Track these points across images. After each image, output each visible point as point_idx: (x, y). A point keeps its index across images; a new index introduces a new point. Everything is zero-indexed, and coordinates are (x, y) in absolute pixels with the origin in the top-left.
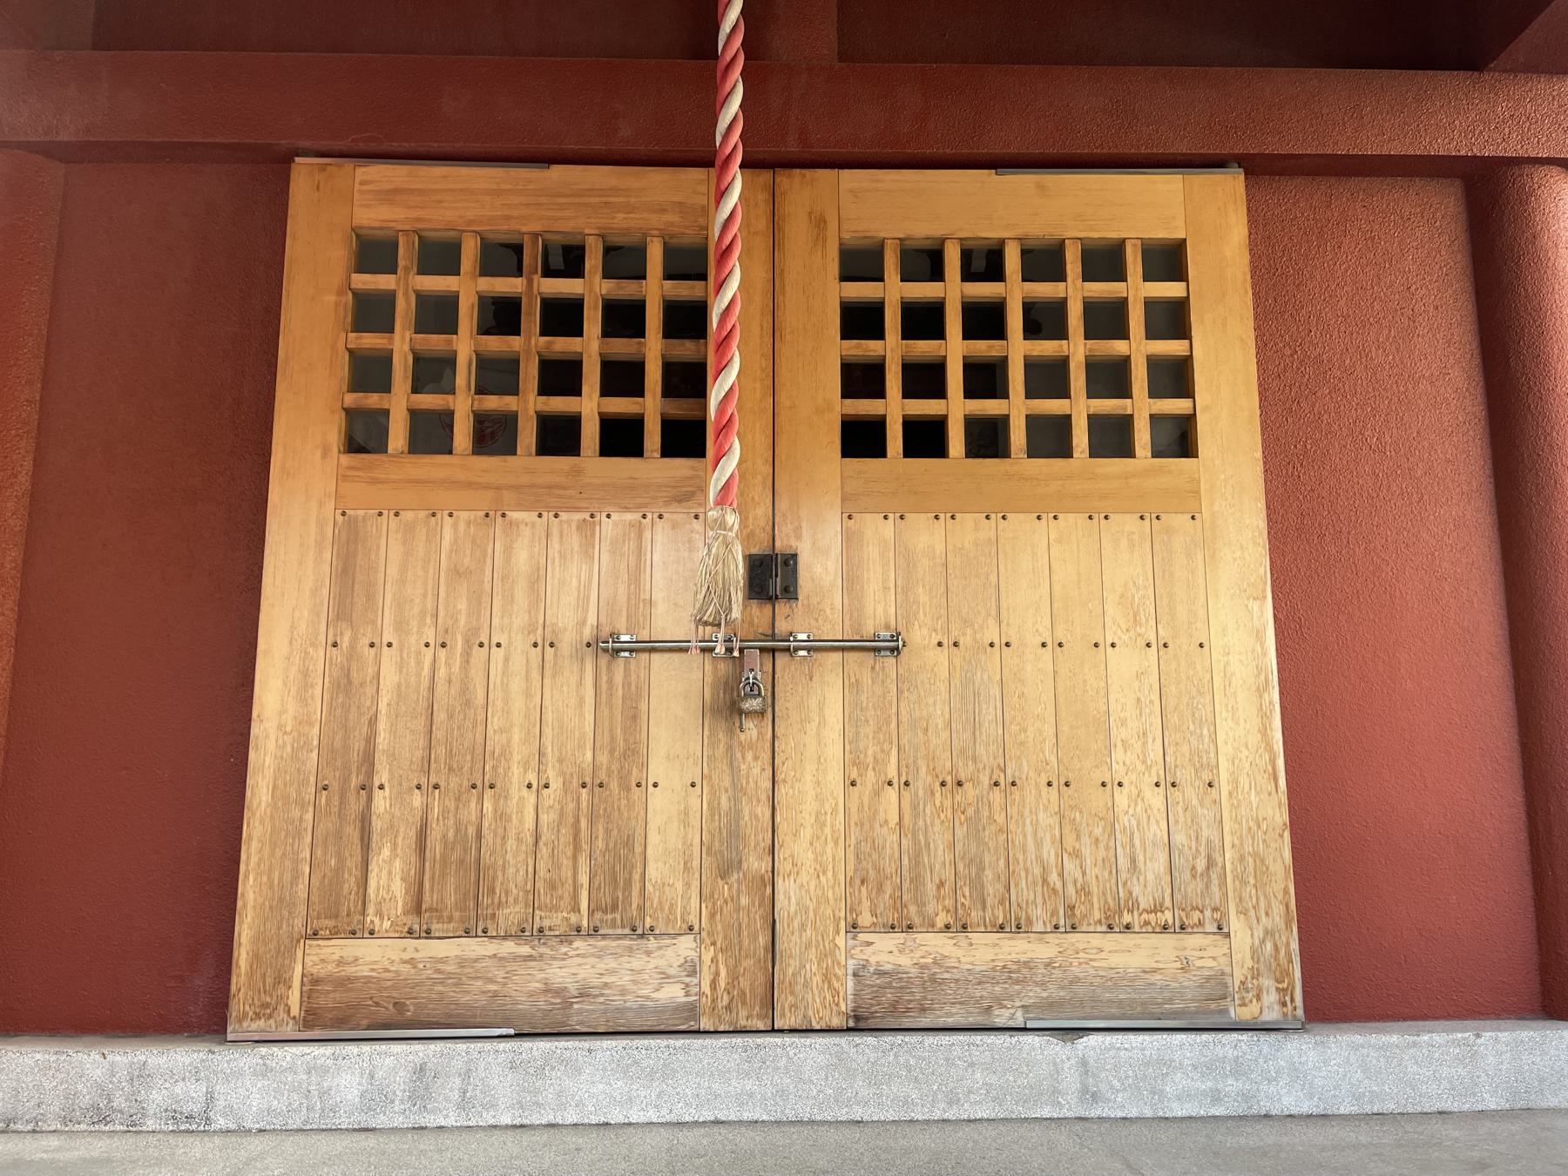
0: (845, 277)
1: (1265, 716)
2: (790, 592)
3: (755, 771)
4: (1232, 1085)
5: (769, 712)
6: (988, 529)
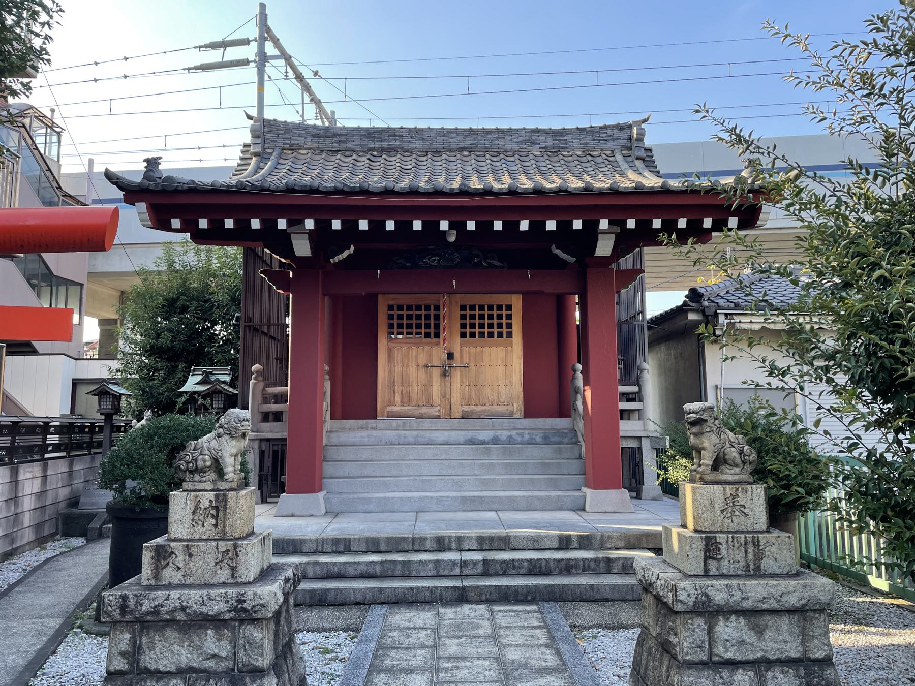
2: (453, 358)
3: (448, 384)
5: (450, 375)
6: (482, 349)
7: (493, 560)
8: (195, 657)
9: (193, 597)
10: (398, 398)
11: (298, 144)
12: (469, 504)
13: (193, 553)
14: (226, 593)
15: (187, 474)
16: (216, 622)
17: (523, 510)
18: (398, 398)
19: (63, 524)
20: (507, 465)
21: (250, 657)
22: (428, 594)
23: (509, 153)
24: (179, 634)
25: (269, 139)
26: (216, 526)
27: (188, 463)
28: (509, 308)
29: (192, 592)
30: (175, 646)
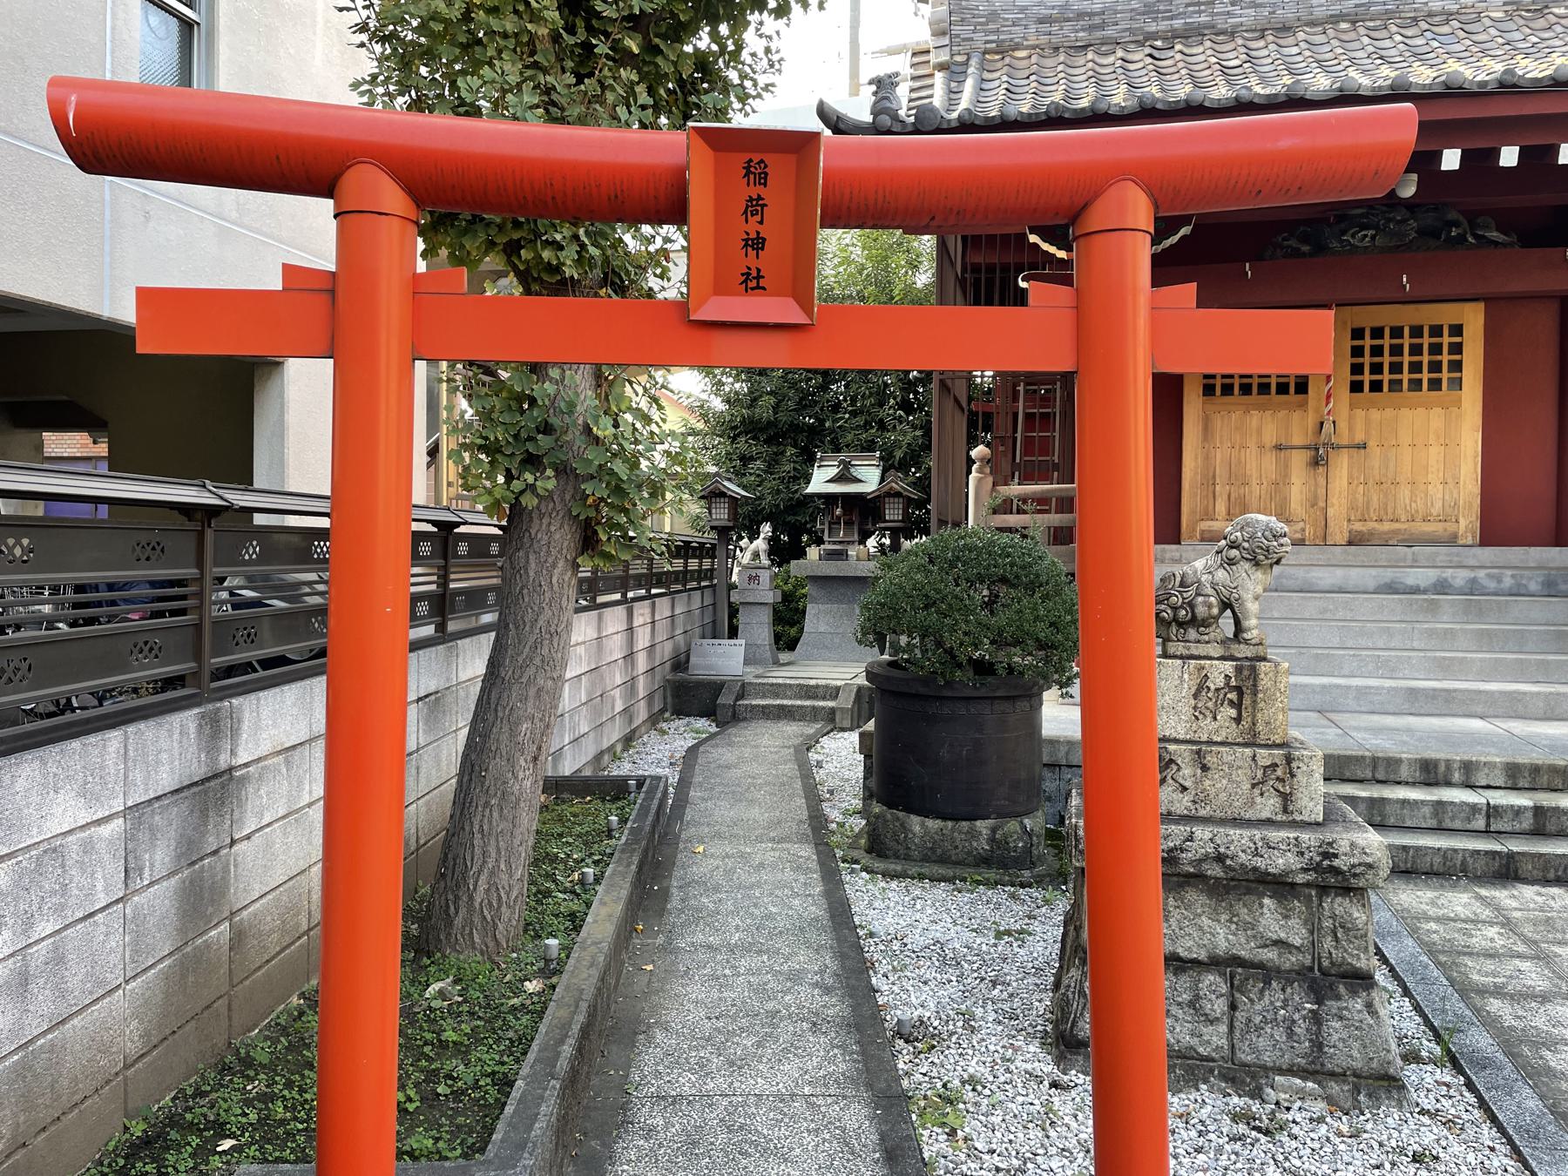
0: (1353, 339)
1: (1476, 464)
3: (1322, 481)
4: (1456, 559)
7: (1557, 809)
8: (1243, 940)
9: (1238, 841)
10: (1221, 507)
11: (1011, 40)
12: (1419, 702)
13: (1209, 765)
14: (1296, 839)
15: (1174, 628)
16: (1279, 886)
17: (1536, 719)
18: (1221, 507)
19: (673, 696)
20: (1482, 632)
21: (1346, 951)
22: (1437, 860)
23: (1437, 19)
24: (1211, 900)
25: (958, 36)
26: (1238, 720)
27: (1175, 609)
28: (1457, 330)
29: (1235, 833)
30: (1203, 918)
